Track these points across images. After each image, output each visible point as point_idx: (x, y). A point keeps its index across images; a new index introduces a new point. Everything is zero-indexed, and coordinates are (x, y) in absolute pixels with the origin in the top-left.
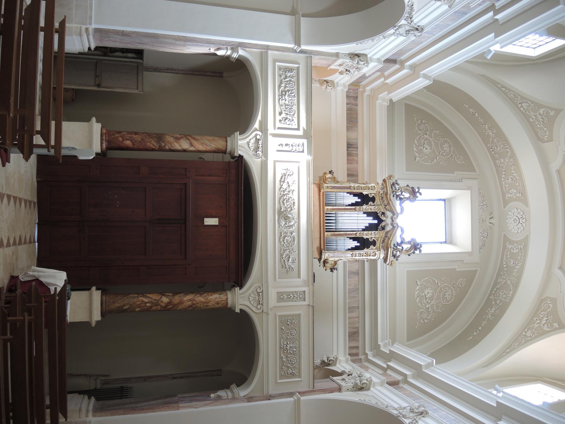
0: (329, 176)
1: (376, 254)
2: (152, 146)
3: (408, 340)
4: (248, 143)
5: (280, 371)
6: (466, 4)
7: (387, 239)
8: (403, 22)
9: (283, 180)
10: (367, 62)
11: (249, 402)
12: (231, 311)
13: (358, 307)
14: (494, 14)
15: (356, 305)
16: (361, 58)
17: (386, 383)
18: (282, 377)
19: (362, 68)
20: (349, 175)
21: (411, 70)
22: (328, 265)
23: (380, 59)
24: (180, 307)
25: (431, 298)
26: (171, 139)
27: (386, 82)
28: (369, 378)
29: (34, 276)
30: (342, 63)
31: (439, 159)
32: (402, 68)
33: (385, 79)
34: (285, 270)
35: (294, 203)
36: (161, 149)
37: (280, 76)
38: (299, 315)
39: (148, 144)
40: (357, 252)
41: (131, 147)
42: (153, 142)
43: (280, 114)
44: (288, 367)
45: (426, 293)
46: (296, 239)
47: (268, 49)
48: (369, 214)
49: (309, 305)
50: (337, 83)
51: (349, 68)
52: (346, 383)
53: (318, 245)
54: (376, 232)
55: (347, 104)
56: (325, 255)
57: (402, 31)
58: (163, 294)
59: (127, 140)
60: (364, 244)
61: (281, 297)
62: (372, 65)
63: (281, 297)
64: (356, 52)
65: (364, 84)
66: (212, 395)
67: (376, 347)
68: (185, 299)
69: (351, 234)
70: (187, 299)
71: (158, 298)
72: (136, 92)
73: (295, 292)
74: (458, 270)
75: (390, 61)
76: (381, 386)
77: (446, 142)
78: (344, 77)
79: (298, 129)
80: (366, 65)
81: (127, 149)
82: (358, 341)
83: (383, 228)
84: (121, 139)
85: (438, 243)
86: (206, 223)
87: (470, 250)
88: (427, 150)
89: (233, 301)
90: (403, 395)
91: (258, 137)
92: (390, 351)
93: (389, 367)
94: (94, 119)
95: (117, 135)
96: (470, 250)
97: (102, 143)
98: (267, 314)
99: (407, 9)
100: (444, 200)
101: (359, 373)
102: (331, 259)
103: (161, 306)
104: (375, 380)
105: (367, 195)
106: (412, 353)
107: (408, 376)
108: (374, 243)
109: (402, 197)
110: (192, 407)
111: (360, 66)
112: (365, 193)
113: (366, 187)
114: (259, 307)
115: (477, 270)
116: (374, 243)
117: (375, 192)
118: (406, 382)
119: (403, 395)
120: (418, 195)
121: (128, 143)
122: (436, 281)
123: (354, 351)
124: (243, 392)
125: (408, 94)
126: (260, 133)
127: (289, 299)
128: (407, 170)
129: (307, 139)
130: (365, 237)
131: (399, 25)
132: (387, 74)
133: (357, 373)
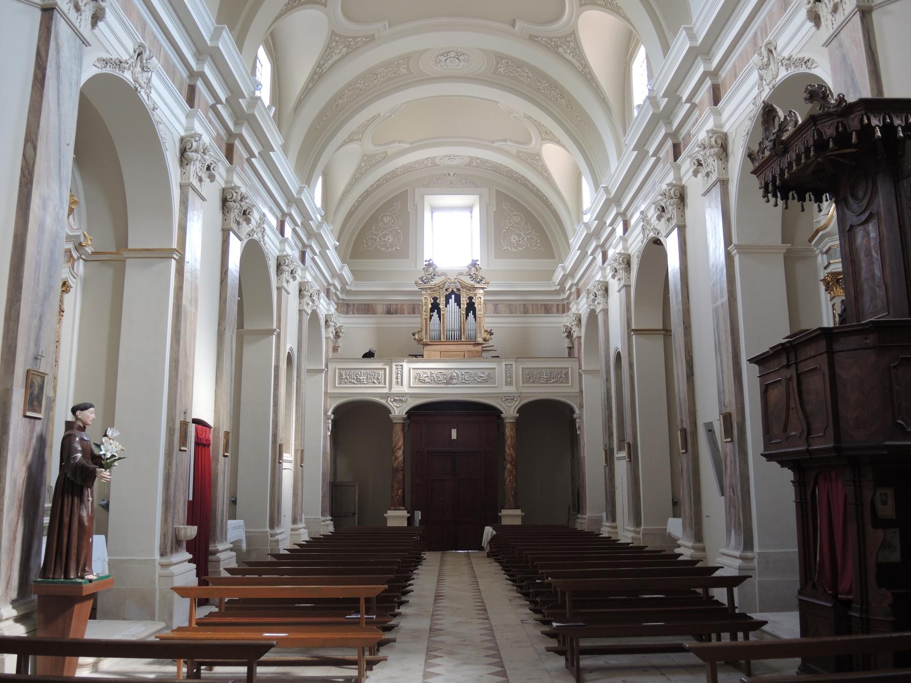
0: (417, 336)
1: (480, 297)
2: (401, 476)
3: (553, 257)
4: (397, 407)
5: (563, 384)
6: (182, 95)
7: (467, 287)
8: (127, 76)
9: (423, 381)
10: (193, 136)
11: (583, 407)
12: (517, 419)
13: (524, 305)
14: (219, 104)
15: (523, 307)
16: (228, 197)
17: (715, 107)
18: (567, 382)
19: (204, 144)
20: (414, 313)
21: (244, 123)
22: (488, 337)
23: (281, 241)
24: (514, 455)
25: (519, 236)
26: (396, 462)
27: (224, 100)
28: (708, 133)
29: (487, 544)
30: (197, 178)
31: (397, 226)
32: (202, 75)
33: (220, 102)
34: (490, 380)
35: (440, 373)
36: (403, 469)
37: (346, 383)
38: (523, 369)
39: (400, 478)
40: (477, 313)
41: (25, 635)
42: (399, 475)
43: (374, 383)
44: (561, 377)
45: (514, 241)
46: (467, 371)
47: (327, 393)
48: (447, 303)
49: (516, 361)
50: (226, 182)
51: (204, 166)
52: (713, 171)
53: (472, 346)
54: (462, 297)
55: (354, 314)
56: (480, 340)
57: (142, 78)
58: (505, 468)
59: (398, 492)
60: (471, 307)
61: (509, 383)
62: (198, 128)
63: (509, 383)
64: (178, 154)
65: (281, 214)
66: (578, 433)
67: (557, 292)
68: (508, 452)
69: (463, 319)
70: (509, 451)
71: (507, 471)
72: (357, 487)
73: (506, 372)
74: (495, 209)
75: (191, 97)
76: (721, 115)
77: (382, 219)
78: (219, 174)
79: (385, 369)
80: (197, 139)
81: (404, 492)
82: (552, 305)
83: (459, 290)
84: (398, 497)
85: (471, 223)
86: (456, 438)
87: (478, 196)
88: (390, 239)
89: (511, 418)
90: (731, 87)
91: (392, 400)
92: (664, 96)
93: (689, 100)
94: (385, 515)
95: (395, 500)
96: (478, 196)
97: (401, 510)
98: (521, 393)
99: (108, 70)
100: (432, 213)
101: (697, 149)
102: (483, 336)
103: (513, 469)
104: (710, 125)
105: (432, 304)
106: (678, 44)
107: (706, 70)
108: (471, 298)
109: (433, 274)
110: (584, 448)
111: (201, 147)
112: (430, 306)
113: (425, 305)
114: (516, 399)
115: (496, 189)
116: (471, 298)
117: (429, 298)
118: (714, 74)
119: (731, 87)
120: (431, 262)
121: (400, 492)
122: (504, 231)
123: (561, 308)
124: (577, 411)
125: (232, 43)
126: (389, 398)
127: (511, 377)
128: (408, 258)
129: (392, 362)
130: (466, 306)
131: (133, 82)
132: (246, 155)
133: (698, 152)
